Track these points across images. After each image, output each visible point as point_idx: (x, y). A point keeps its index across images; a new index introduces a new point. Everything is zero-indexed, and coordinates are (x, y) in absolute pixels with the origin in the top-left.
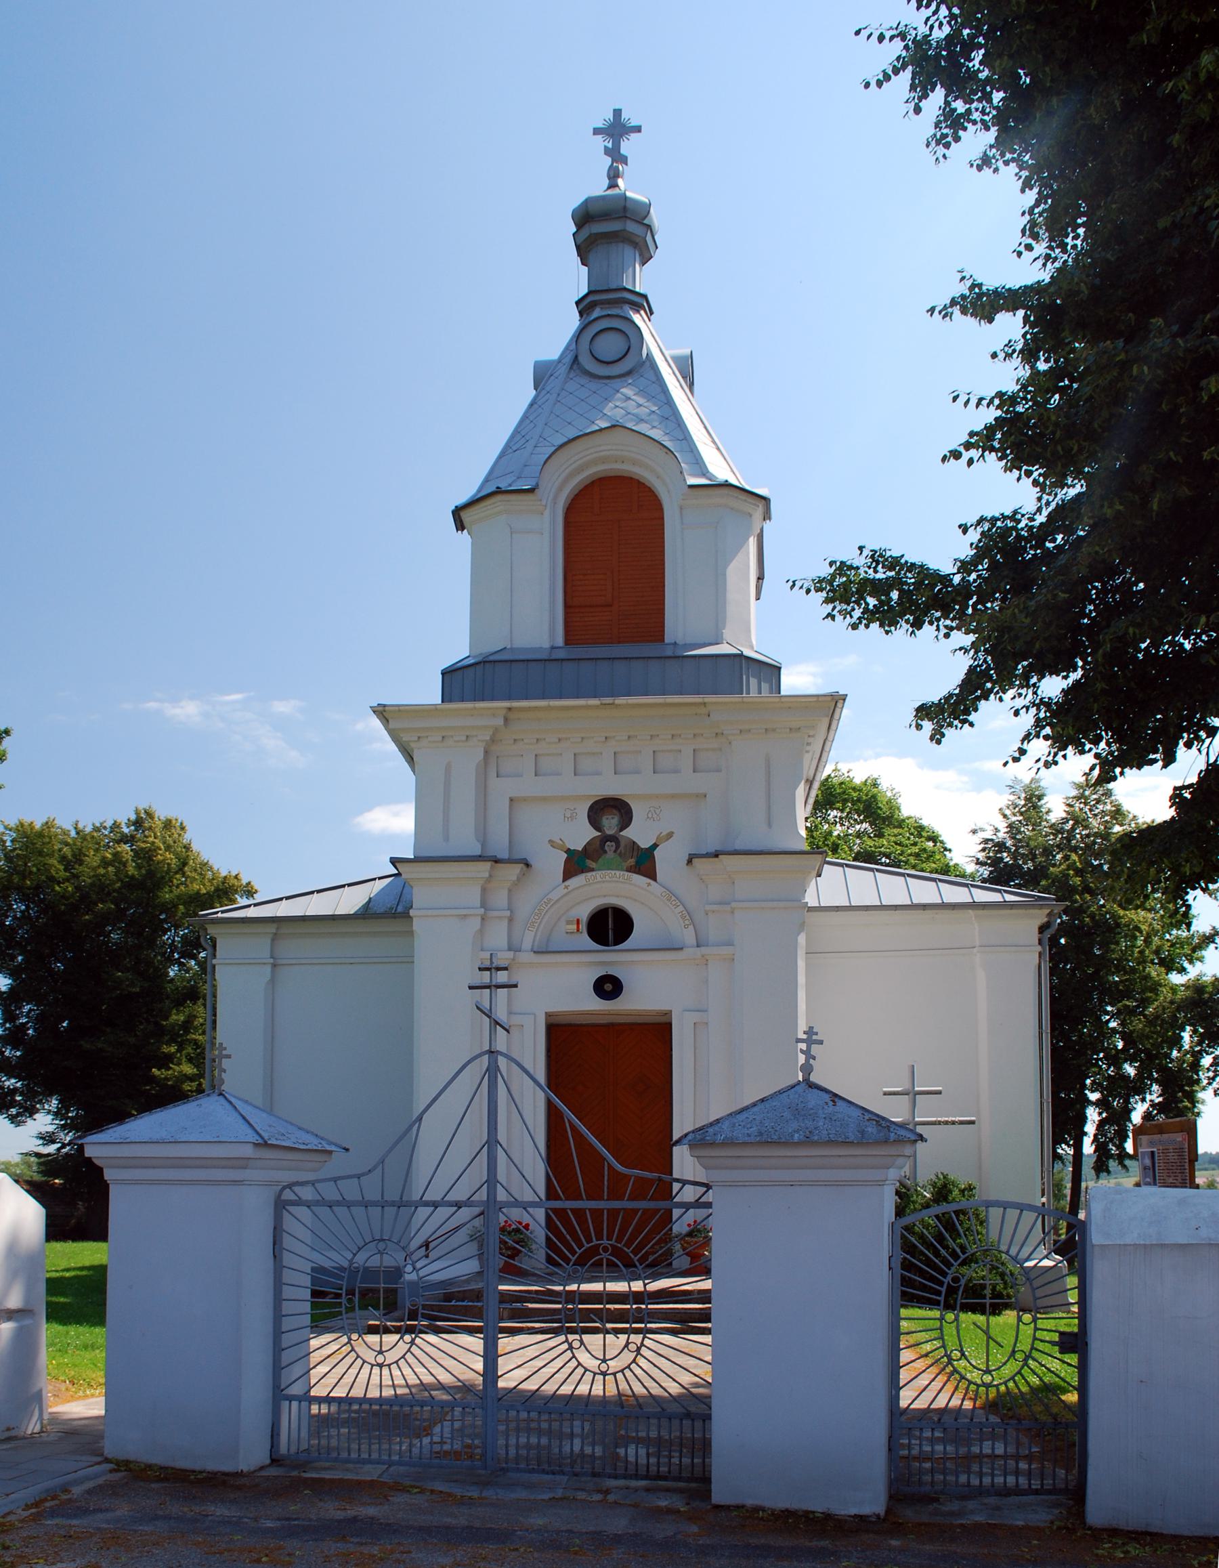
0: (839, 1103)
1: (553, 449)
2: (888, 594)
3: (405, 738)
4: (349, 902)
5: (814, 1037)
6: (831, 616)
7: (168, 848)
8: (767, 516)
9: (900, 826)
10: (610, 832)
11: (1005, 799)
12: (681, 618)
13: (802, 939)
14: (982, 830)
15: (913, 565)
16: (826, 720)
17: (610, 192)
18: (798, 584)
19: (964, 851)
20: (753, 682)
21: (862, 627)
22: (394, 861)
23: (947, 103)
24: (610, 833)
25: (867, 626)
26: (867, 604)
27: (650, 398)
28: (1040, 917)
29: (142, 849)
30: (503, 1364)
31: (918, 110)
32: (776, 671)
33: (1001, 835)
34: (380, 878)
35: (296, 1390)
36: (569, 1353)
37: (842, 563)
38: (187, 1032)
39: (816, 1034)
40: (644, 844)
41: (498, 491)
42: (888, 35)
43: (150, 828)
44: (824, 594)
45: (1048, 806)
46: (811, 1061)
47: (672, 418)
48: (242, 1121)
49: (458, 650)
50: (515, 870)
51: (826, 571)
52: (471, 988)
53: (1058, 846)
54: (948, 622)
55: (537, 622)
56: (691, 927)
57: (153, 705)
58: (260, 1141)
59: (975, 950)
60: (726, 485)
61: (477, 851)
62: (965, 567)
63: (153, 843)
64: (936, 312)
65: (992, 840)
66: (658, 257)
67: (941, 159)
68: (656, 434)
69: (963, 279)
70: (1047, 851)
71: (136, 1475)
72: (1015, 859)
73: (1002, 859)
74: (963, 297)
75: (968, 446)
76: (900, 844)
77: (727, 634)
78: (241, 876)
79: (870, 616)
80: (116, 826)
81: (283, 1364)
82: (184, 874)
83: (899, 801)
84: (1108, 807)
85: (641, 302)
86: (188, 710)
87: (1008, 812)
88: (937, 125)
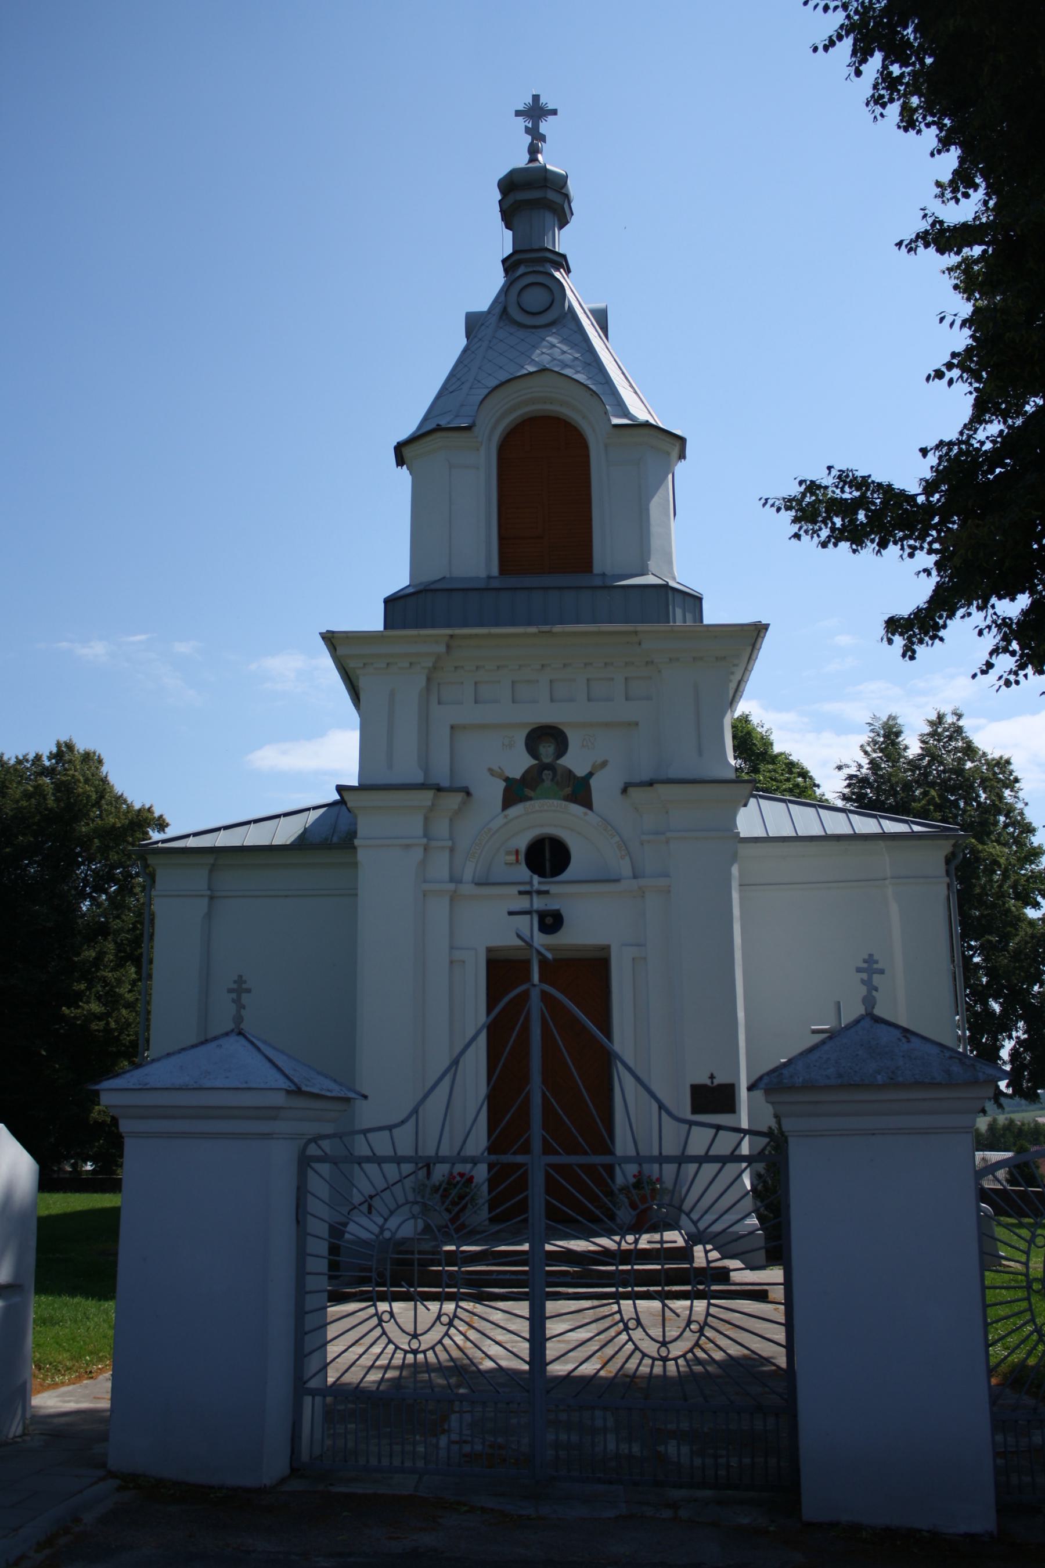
0: (913, 1039)
1: (486, 391)
2: (849, 513)
3: (351, 664)
4: (286, 833)
5: (875, 966)
6: (797, 536)
7: (87, 781)
8: (682, 456)
9: (774, 763)
10: (547, 760)
11: (865, 738)
12: (607, 551)
13: (735, 870)
14: (848, 766)
15: (880, 485)
16: (749, 649)
17: (530, 165)
18: (770, 502)
19: (832, 786)
20: (679, 612)
21: (831, 545)
22: (340, 789)
23: (885, 67)
24: (547, 767)
25: (835, 545)
26: (834, 524)
27: (573, 345)
28: (946, 847)
29: (63, 782)
30: (552, 1349)
31: (858, 73)
32: (697, 602)
33: (864, 771)
34: (315, 808)
35: (313, 1384)
36: (624, 1337)
37: (812, 482)
38: (98, 969)
39: (877, 962)
40: (580, 772)
41: (439, 429)
42: (832, 5)
43: (70, 761)
44: (793, 513)
45: (905, 742)
46: (874, 993)
47: (594, 364)
48: (268, 1065)
49: (399, 579)
50: (454, 800)
51: (796, 490)
52: (511, 913)
53: (917, 782)
54: (911, 542)
55: (475, 555)
56: (627, 858)
57: (64, 645)
58: (293, 1088)
59: (887, 882)
60: (647, 425)
61: (419, 779)
62: (930, 487)
63: (73, 776)
64: (903, 247)
65: (856, 776)
66: (574, 221)
67: (879, 117)
68: (581, 377)
69: (925, 216)
70: (907, 786)
71: (152, 1495)
72: (878, 795)
73: (867, 794)
74: (926, 232)
75: (950, 366)
76: (775, 780)
77: (652, 565)
78: (154, 809)
79: (837, 536)
80: (38, 758)
81: (307, 1350)
82: (100, 808)
83: (772, 737)
84: (960, 744)
85: (561, 262)
86: (97, 650)
87: (869, 749)
88: (875, 87)
